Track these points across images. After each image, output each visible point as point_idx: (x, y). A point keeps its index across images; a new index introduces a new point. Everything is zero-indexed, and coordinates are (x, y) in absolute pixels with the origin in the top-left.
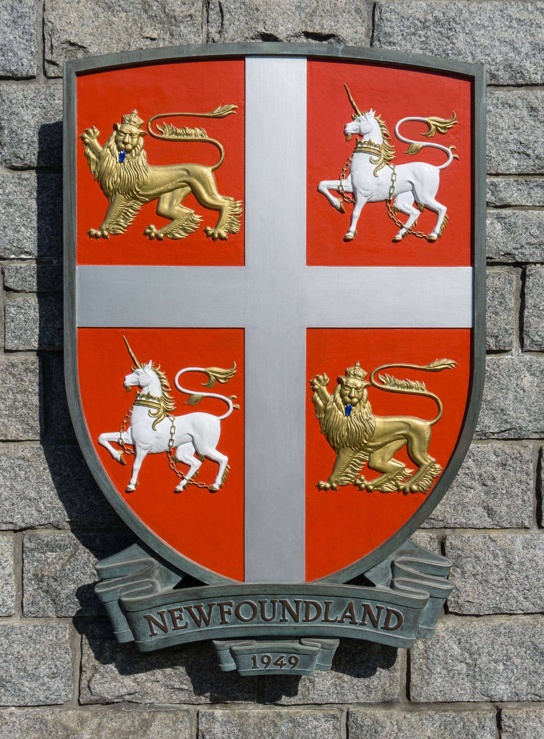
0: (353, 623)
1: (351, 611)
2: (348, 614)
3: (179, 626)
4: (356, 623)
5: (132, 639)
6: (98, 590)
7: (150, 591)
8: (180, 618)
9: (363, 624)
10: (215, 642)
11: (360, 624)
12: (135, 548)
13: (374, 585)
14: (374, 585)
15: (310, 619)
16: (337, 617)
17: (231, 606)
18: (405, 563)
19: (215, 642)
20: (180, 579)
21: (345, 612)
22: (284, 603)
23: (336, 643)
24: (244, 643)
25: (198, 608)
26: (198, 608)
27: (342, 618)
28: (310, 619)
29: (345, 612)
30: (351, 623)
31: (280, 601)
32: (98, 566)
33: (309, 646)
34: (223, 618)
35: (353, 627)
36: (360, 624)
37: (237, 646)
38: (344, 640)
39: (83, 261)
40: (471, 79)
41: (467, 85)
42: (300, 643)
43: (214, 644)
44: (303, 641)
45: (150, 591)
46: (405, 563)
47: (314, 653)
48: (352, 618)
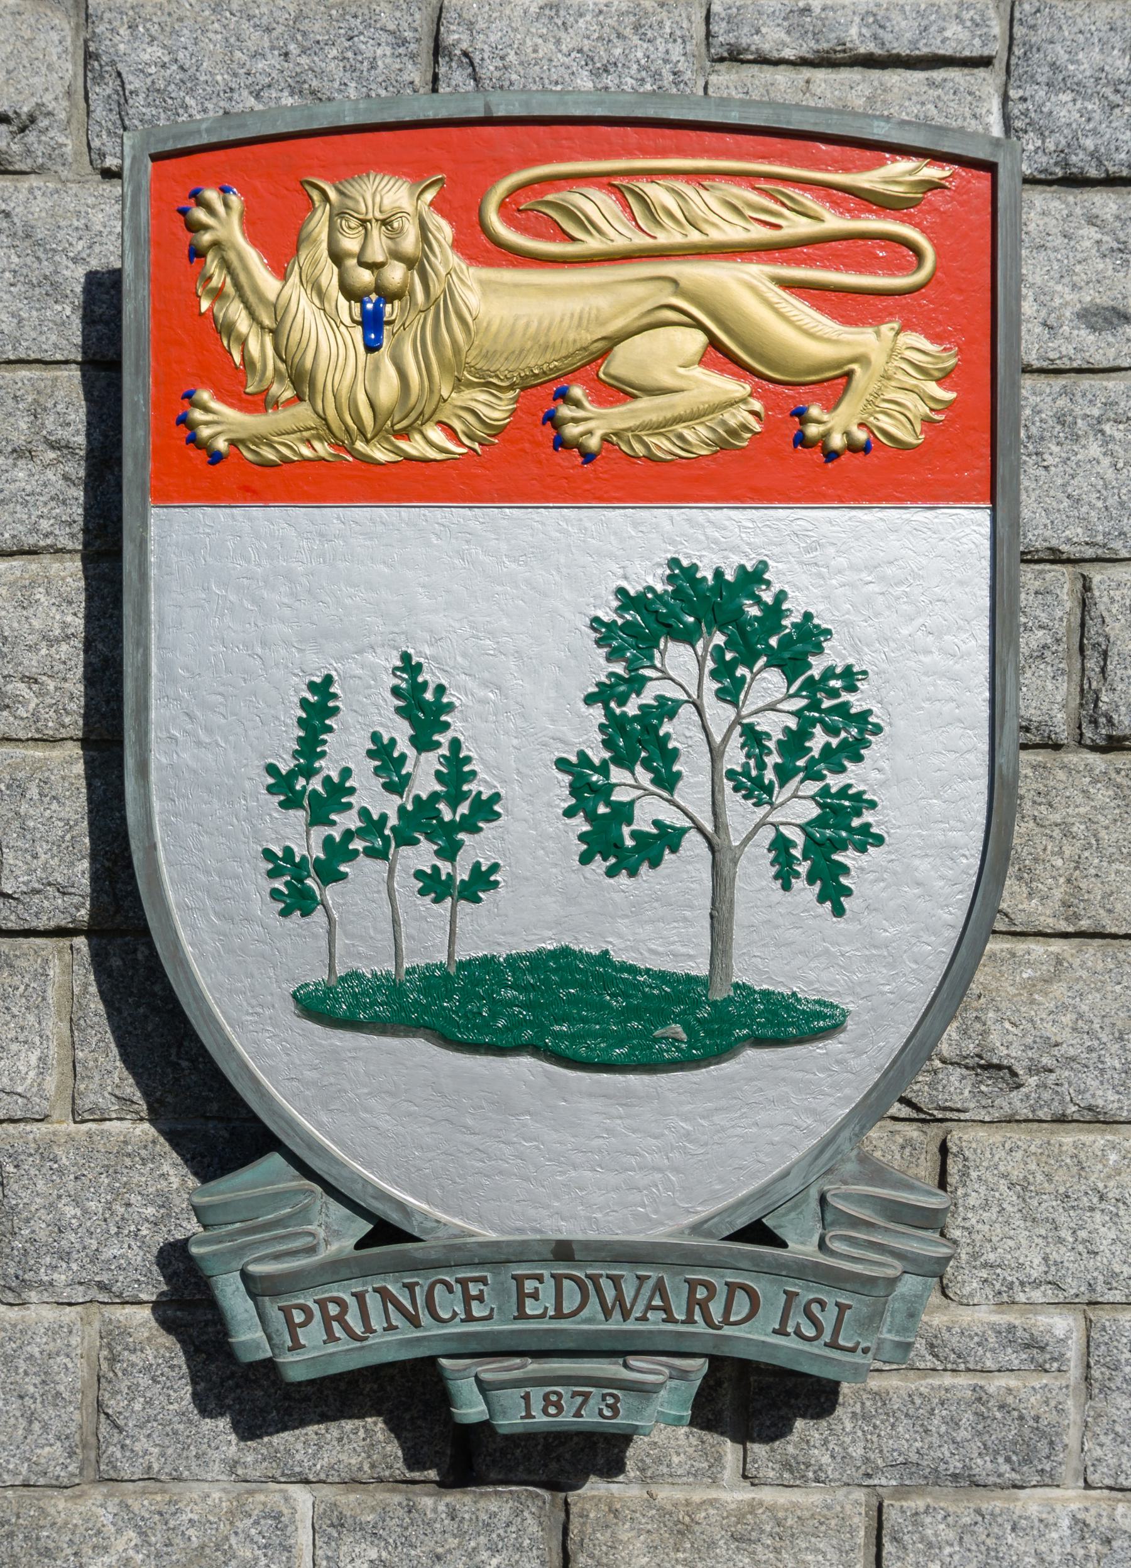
0: (670, 1319)
1: (664, 1297)
2: (657, 1302)
3: (529, 1312)
4: (676, 1321)
5: (269, 1354)
6: (194, 1250)
7: (312, 1250)
8: (535, 1296)
9: (690, 1320)
10: (444, 1362)
11: (683, 1322)
12: (274, 1161)
13: (784, 1245)
14: (784, 1245)
15: (566, 1311)
16: (546, 1308)
17: (486, 1284)
18: (847, 1197)
19: (444, 1362)
20: (365, 1227)
21: (651, 1298)
22: (383, 1292)
23: (699, 1366)
24: (506, 1364)
25: (616, 1281)
26: (616, 1281)
27: (646, 1312)
28: (566, 1311)
29: (651, 1298)
30: (664, 1321)
31: (375, 1290)
32: (197, 1200)
33: (644, 1370)
34: (521, 1306)
35: (670, 1327)
36: (683, 1322)
37: (491, 1370)
38: (716, 1362)
39: (167, 495)
40: (990, 167)
41: (980, 182)
42: (626, 1365)
43: (442, 1367)
44: (633, 1361)
45: (312, 1250)
46: (847, 1197)
47: (655, 1388)
48: (666, 1309)
